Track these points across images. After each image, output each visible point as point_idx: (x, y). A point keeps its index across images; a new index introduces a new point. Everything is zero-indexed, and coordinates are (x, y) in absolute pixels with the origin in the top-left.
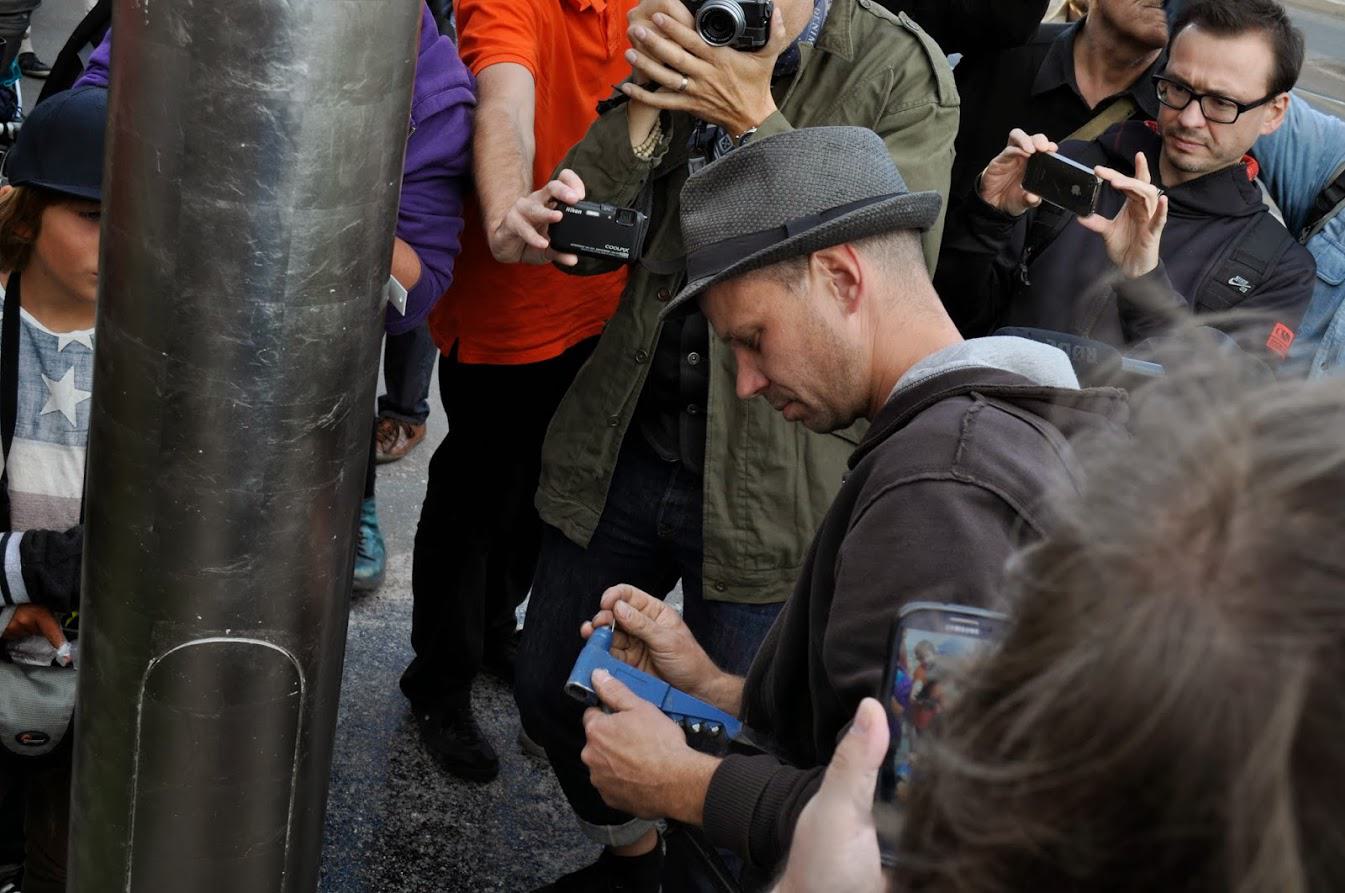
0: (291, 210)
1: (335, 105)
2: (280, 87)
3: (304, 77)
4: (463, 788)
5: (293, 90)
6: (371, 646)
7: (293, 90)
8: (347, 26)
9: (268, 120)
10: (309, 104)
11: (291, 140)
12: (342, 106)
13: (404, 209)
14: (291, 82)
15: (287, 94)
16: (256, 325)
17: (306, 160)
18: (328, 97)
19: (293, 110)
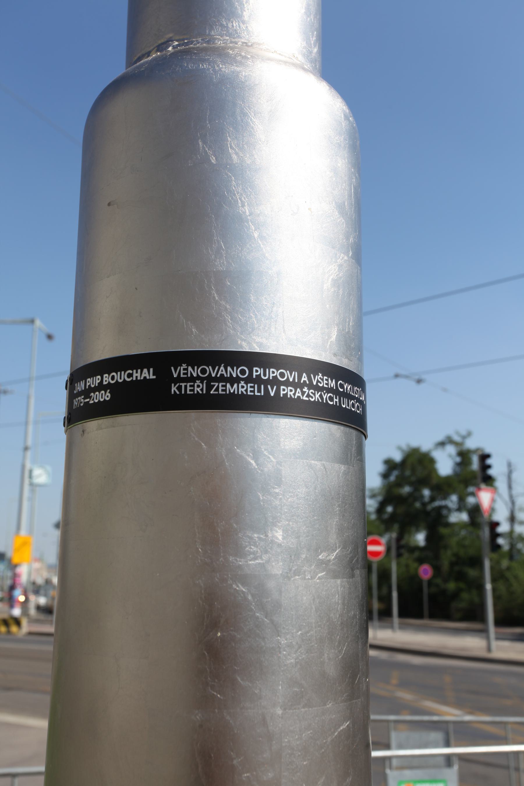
0: (279, 712)
1: (312, 578)
2: (255, 559)
3: (279, 545)
4: (337, 214)
5: (268, 561)
6: (320, 335)
7: (268, 561)
8: (315, 488)
9: (246, 599)
10: (287, 577)
11: (272, 622)
12: (319, 578)
13: (386, 600)
14: (266, 552)
15: (262, 566)
16: (248, 164)
17: (290, 646)
18: (305, 568)
19: (271, 584)
